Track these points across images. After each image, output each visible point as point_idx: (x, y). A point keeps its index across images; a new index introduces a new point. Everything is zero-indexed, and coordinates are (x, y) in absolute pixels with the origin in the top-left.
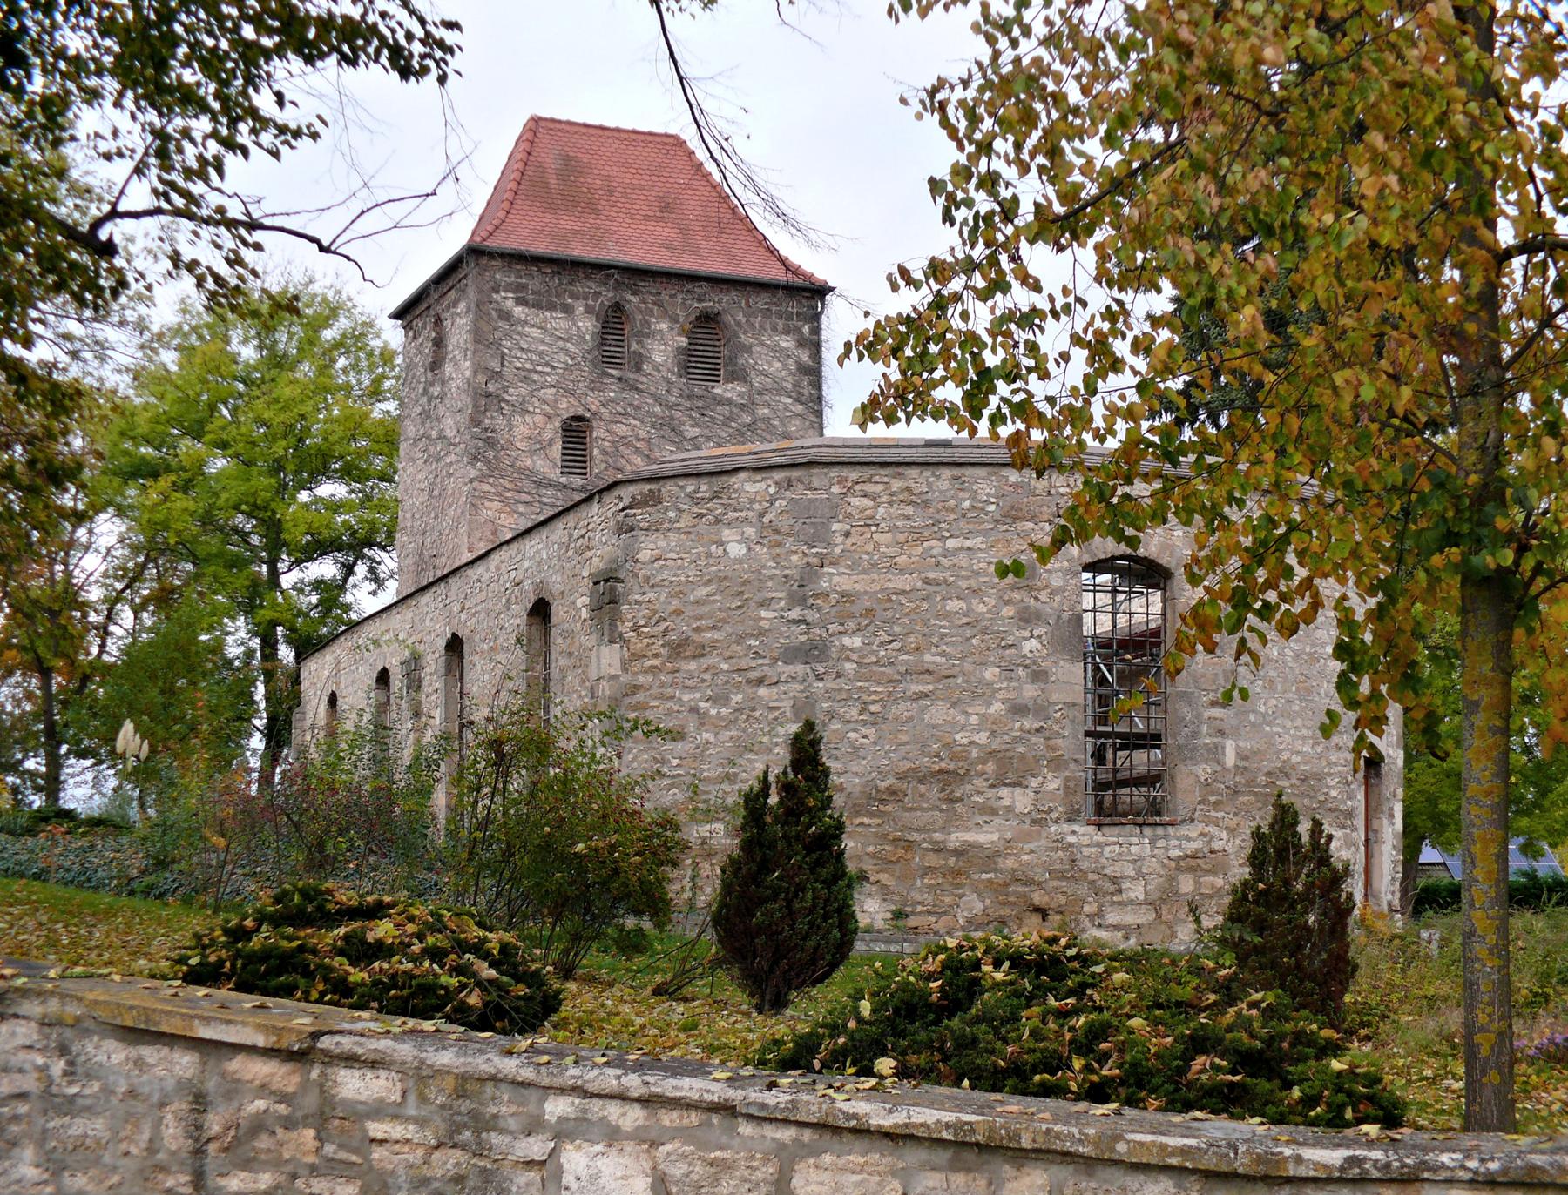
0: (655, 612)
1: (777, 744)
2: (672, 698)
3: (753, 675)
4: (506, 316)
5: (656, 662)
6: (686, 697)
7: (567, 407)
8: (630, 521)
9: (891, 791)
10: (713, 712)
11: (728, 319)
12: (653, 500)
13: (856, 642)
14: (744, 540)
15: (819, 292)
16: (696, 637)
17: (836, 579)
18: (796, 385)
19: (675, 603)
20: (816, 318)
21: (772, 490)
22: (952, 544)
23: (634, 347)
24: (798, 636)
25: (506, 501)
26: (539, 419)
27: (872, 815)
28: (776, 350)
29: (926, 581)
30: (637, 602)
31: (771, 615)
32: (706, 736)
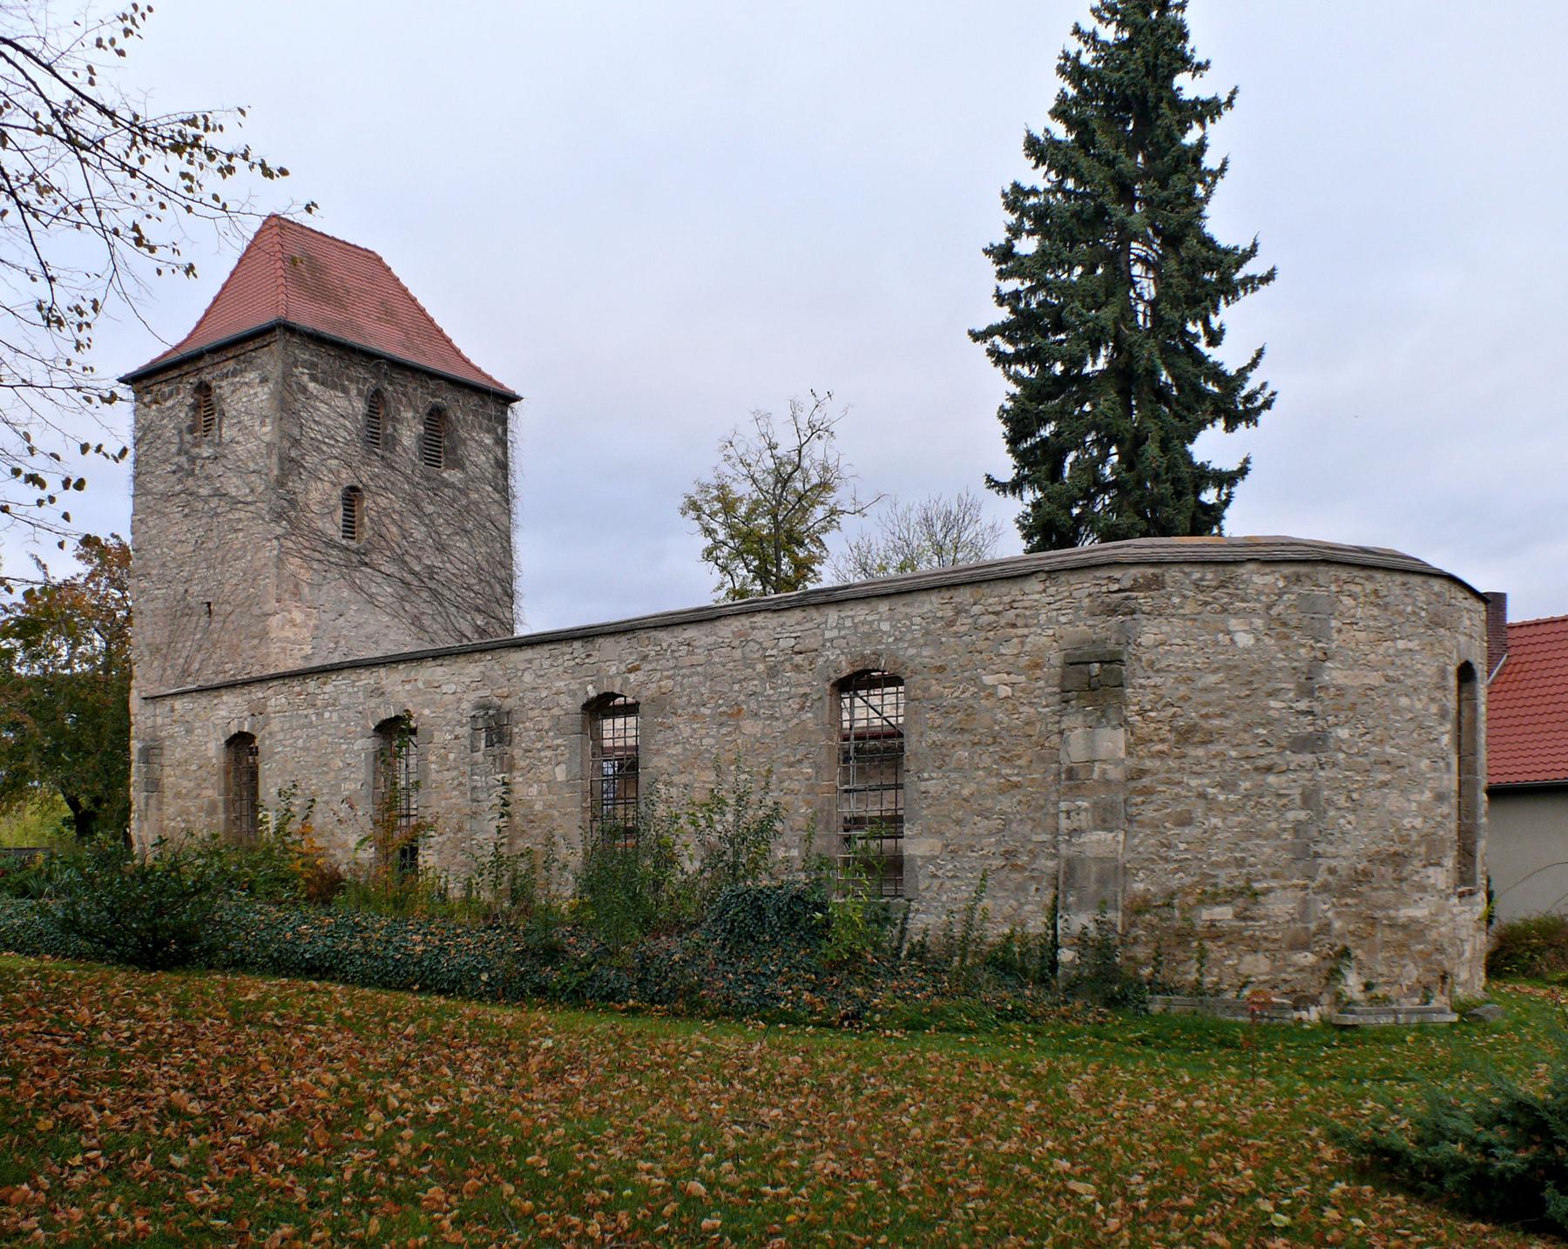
0: (1162, 697)
1: (1285, 830)
2: (1179, 783)
3: (1261, 763)
4: (304, 390)
5: (1160, 747)
6: (1194, 782)
7: (347, 478)
8: (1132, 604)
9: (1365, 873)
10: (1222, 798)
11: (451, 414)
12: (1155, 584)
13: (1343, 733)
14: (1253, 631)
15: (507, 399)
16: (1203, 723)
17: (1334, 673)
18: (495, 477)
19: (1183, 690)
20: (504, 421)
21: (1281, 584)
22: (1401, 644)
23: (390, 430)
24: (1305, 726)
25: (303, 558)
26: (327, 485)
27: (1353, 895)
28: (480, 443)
29: (1388, 679)
30: (1142, 686)
31: (1279, 705)
32: (1214, 821)
